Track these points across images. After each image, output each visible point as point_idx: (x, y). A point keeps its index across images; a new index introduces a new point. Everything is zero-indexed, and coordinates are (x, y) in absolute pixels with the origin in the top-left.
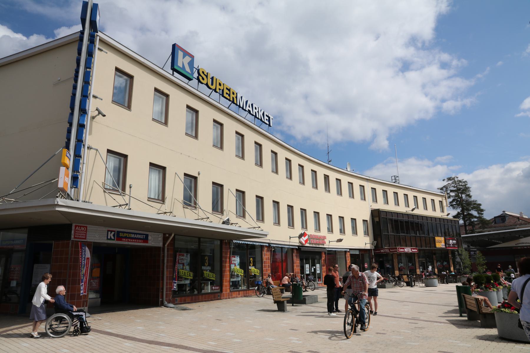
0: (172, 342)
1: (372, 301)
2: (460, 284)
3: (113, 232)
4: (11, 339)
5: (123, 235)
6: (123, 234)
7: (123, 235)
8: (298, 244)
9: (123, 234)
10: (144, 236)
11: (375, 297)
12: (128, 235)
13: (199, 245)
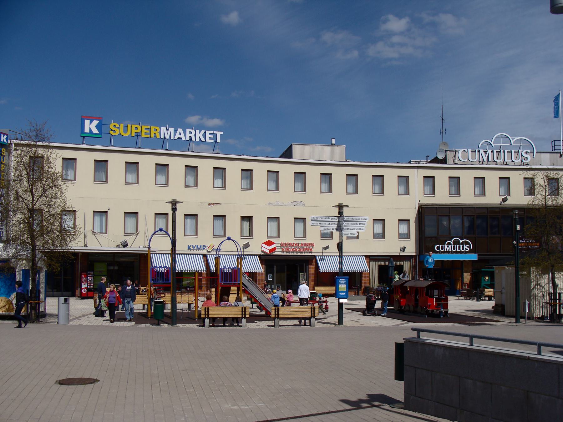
0: (467, 314)
1: (399, 277)
2: (9, 148)
3: (95, 121)
4: (373, 409)
5: (126, 131)
6: (126, 126)
7: (126, 131)
8: (259, 254)
9: (126, 126)
10: (219, 133)
11: (107, 163)
12: (144, 131)
13: (173, 261)
